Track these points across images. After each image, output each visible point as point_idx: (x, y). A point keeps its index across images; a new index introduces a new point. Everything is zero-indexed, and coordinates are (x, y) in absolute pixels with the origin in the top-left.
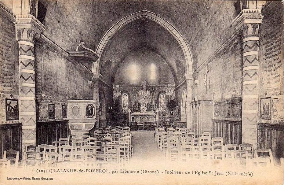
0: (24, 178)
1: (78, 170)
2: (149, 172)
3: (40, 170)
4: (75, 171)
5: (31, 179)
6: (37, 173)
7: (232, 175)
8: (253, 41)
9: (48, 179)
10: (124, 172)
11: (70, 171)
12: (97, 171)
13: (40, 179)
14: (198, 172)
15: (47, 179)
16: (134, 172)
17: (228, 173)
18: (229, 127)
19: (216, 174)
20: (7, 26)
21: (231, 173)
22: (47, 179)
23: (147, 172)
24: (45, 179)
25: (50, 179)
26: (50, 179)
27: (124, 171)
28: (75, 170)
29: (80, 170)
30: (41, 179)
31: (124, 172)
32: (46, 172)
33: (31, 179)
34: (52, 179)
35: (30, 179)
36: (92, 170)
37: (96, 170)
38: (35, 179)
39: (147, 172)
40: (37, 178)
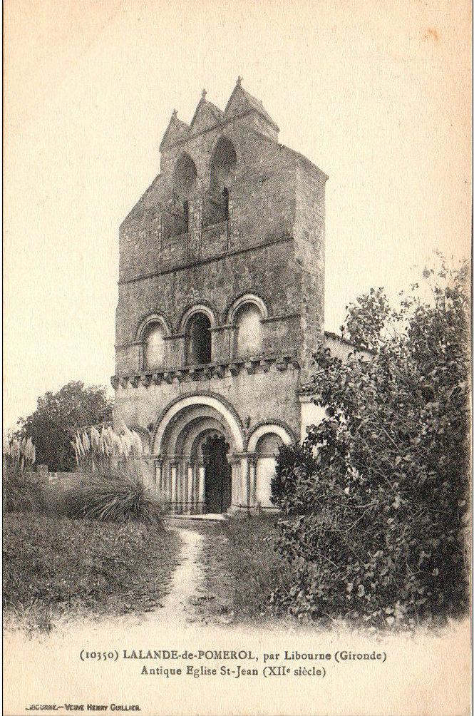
0: (69, 707)
1: (181, 652)
2: (356, 657)
3: (87, 653)
4: (175, 657)
5: (85, 708)
6: (83, 660)
7: (279, 674)
8: (180, 274)
9: (128, 708)
10: (295, 657)
11: (162, 656)
12: (226, 657)
13: (106, 708)
14: (193, 670)
15: (124, 708)
16: (318, 657)
17: (268, 671)
18: (191, 485)
19: (241, 674)
20: (169, 181)
21: (276, 671)
22: (124, 708)
23: (352, 656)
24: (120, 708)
25: (132, 708)
26: (132, 708)
27: (295, 654)
28: (175, 653)
29: (186, 654)
30: (109, 708)
31: (295, 657)
32: (103, 658)
33: (85, 708)
34: (137, 708)
35: (81, 708)
36: (214, 653)
37: (222, 654)
38: (94, 710)
39: (352, 656)
40: (100, 705)
